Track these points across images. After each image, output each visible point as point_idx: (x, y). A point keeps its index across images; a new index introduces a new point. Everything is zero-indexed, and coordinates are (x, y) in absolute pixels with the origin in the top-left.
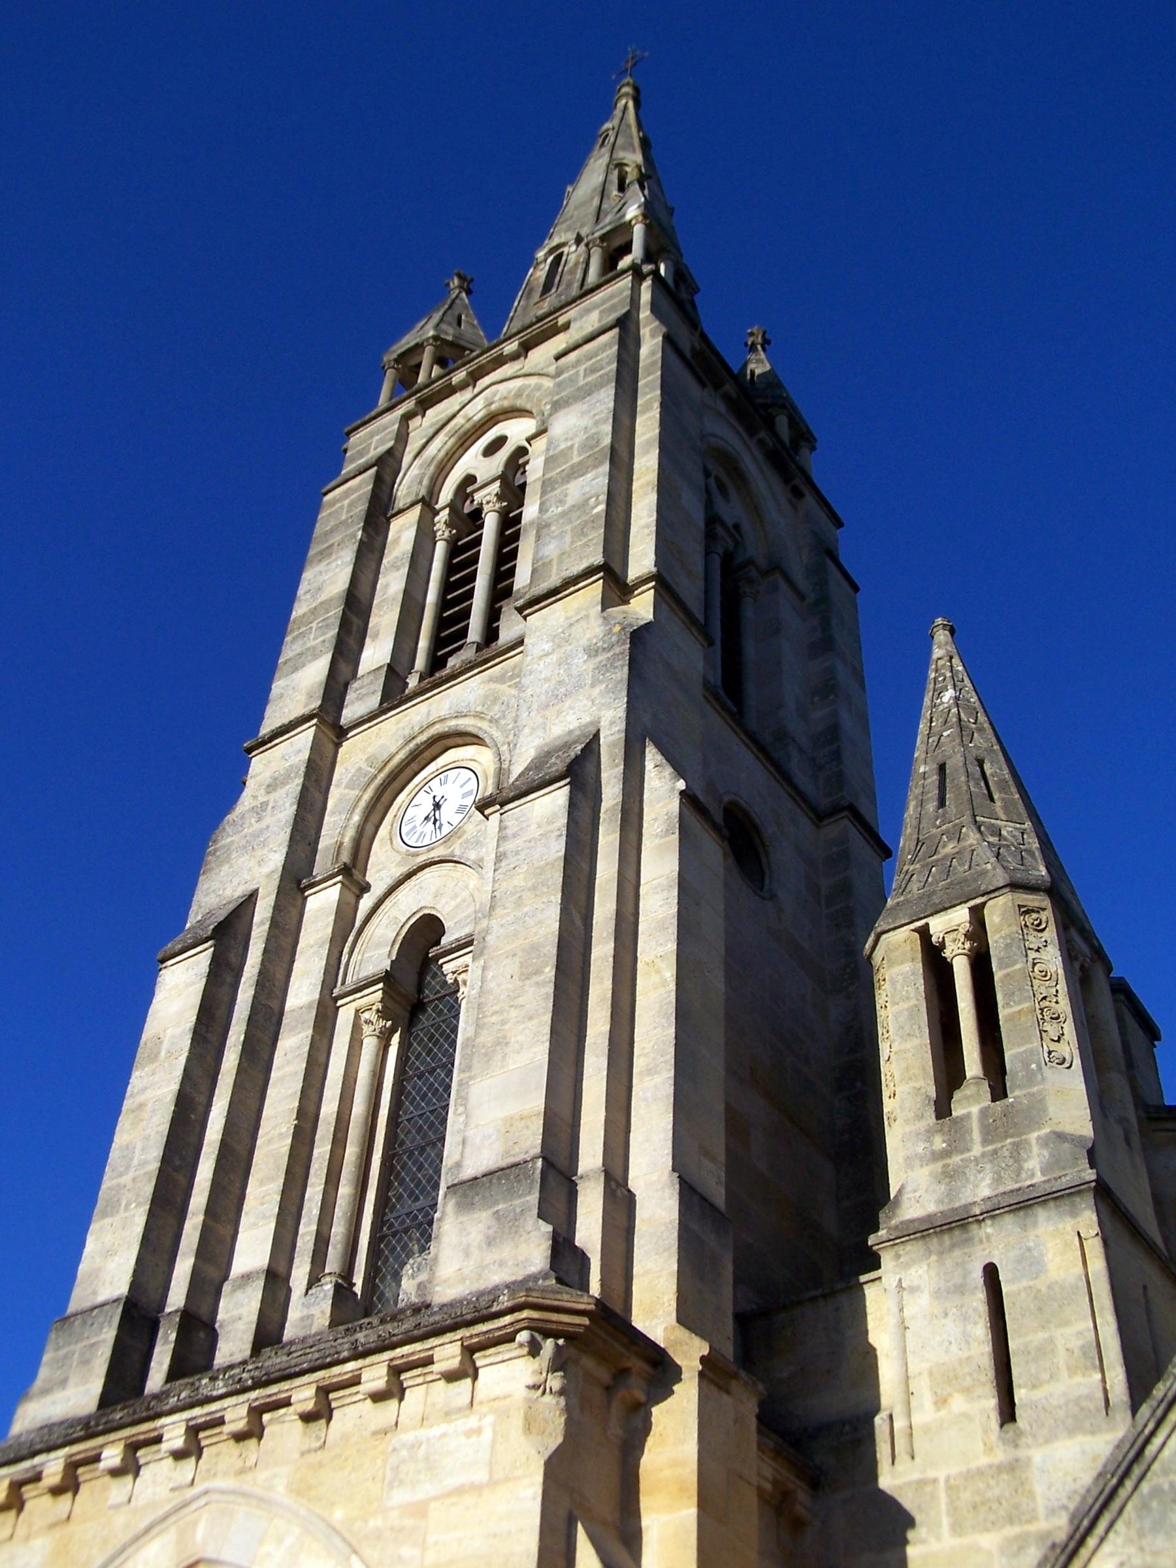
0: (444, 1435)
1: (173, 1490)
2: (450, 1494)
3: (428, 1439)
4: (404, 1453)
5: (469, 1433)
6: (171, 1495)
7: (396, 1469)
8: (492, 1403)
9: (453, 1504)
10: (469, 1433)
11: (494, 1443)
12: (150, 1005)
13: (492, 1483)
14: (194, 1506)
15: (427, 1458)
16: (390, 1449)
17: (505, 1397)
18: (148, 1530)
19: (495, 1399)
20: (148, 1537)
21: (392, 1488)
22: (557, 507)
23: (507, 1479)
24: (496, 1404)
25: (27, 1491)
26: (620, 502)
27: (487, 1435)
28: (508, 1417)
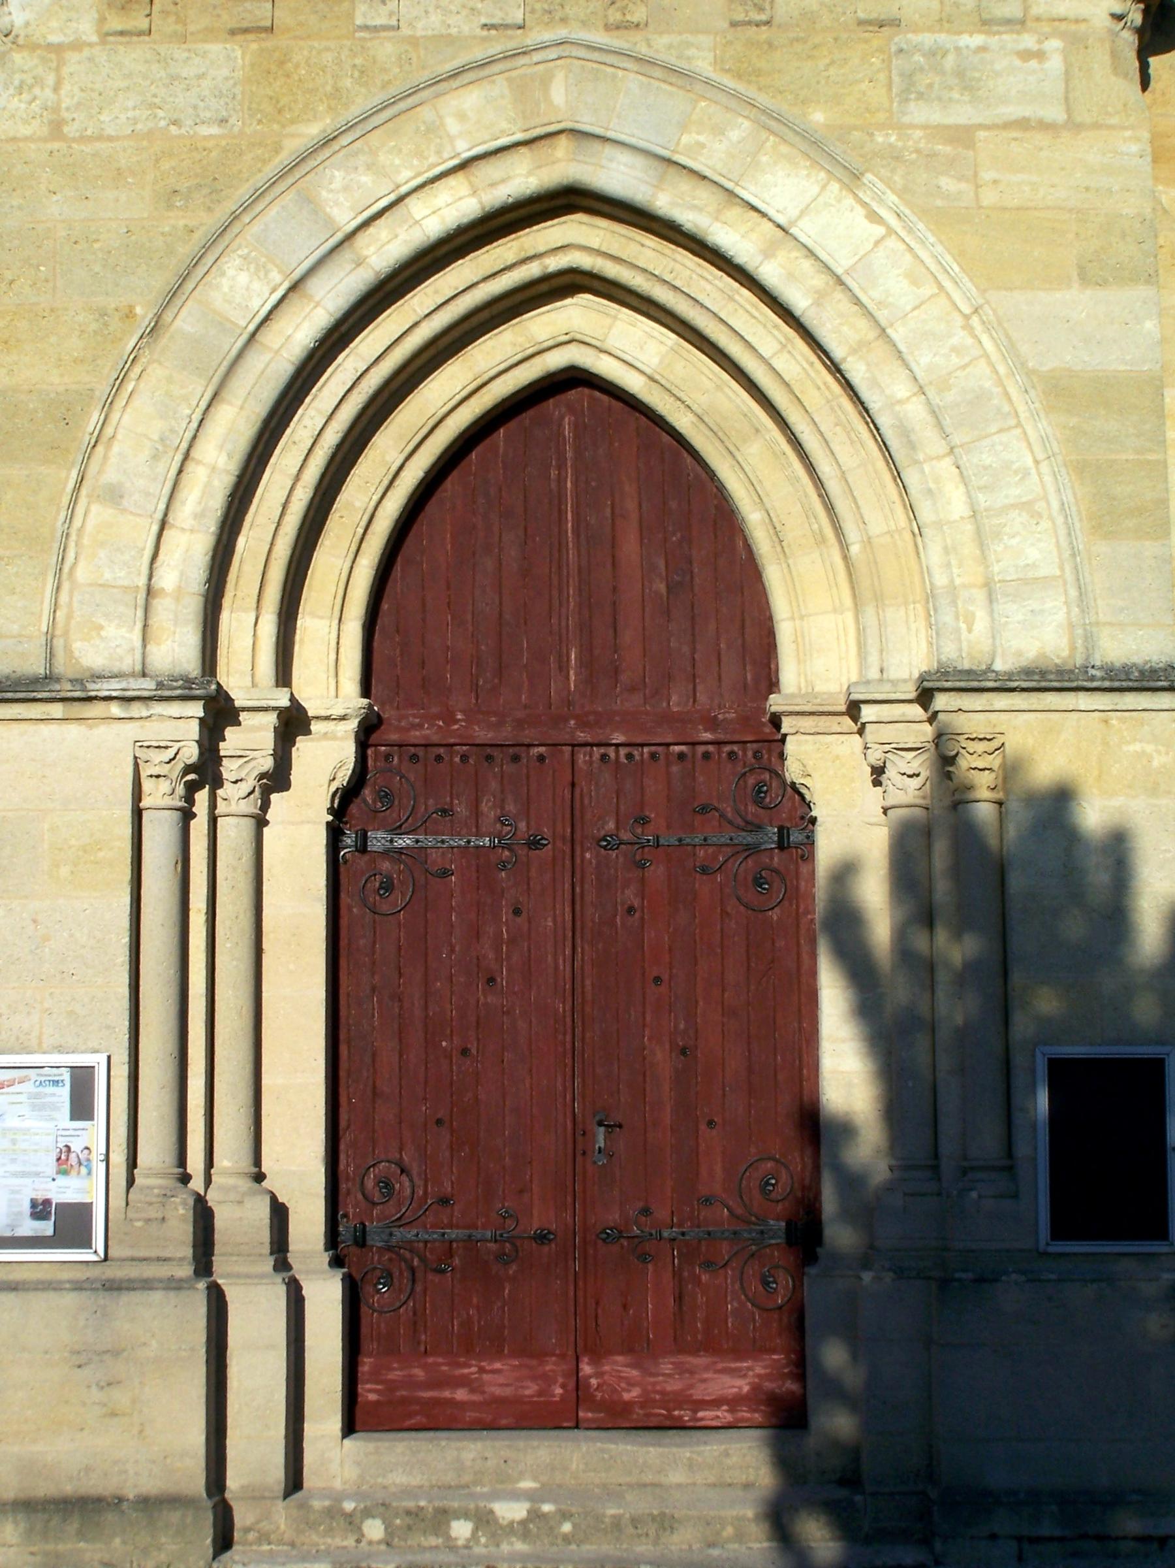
0: (983, 49)
1: (485, 26)
2: (1007, 126)
3: (957, 49)
4: (918, 58)
5: (1026, 55)
6: (479, 32)
7: (909, 77)
8: (1057, 23)
9: (1015, 139)
10: (1026, 55)
11: (1068, 76)
12: (233, 555)
13: (1073, 126)
14: (536, 57)
15: (960, 73)
16: (894, 48)
17: (1077, 21)
18: (455, 75)
19: (1060, 20)
20: (455, 83)
21: (907, 100)
22: (595, 7)
23: (1097, 126)
24: (1063, 26)
25: (301, 741)
26: (665, 231)
27: (1055, 63)
28: (1086, 48)
